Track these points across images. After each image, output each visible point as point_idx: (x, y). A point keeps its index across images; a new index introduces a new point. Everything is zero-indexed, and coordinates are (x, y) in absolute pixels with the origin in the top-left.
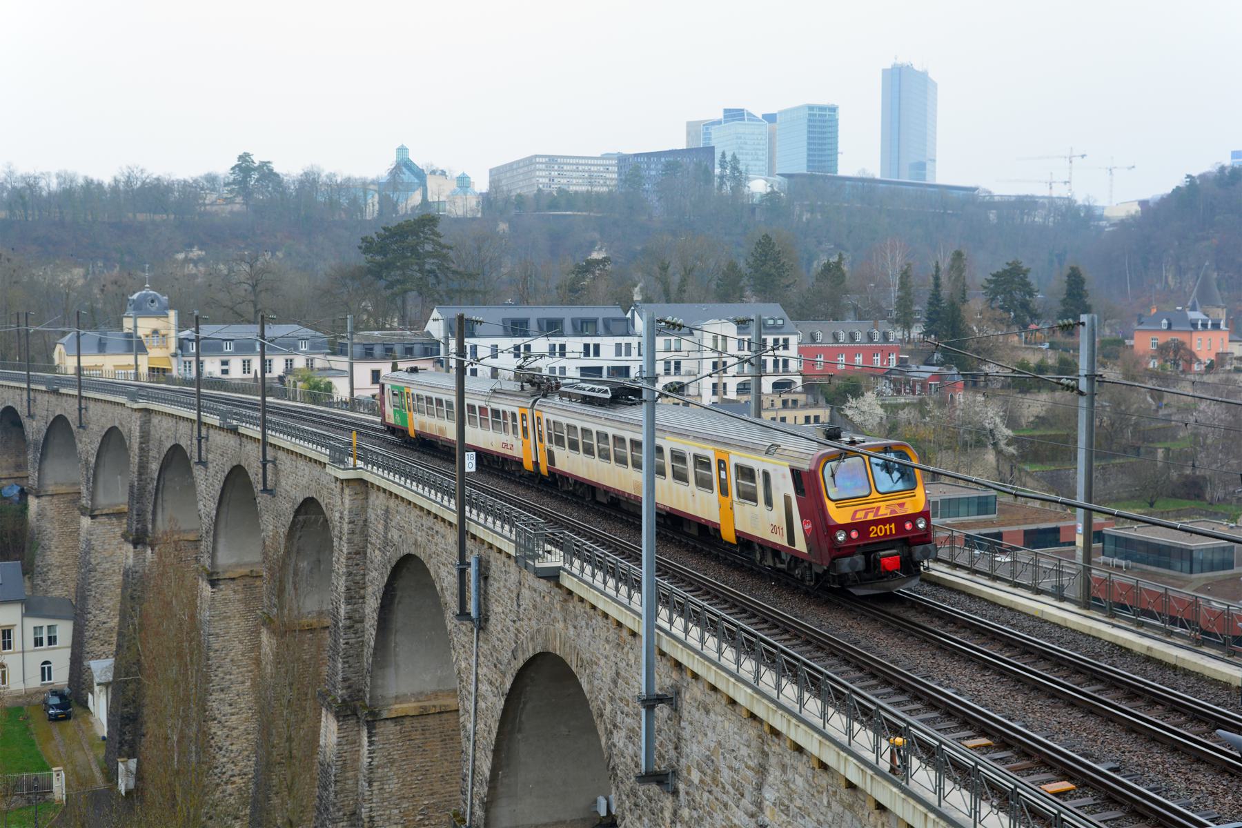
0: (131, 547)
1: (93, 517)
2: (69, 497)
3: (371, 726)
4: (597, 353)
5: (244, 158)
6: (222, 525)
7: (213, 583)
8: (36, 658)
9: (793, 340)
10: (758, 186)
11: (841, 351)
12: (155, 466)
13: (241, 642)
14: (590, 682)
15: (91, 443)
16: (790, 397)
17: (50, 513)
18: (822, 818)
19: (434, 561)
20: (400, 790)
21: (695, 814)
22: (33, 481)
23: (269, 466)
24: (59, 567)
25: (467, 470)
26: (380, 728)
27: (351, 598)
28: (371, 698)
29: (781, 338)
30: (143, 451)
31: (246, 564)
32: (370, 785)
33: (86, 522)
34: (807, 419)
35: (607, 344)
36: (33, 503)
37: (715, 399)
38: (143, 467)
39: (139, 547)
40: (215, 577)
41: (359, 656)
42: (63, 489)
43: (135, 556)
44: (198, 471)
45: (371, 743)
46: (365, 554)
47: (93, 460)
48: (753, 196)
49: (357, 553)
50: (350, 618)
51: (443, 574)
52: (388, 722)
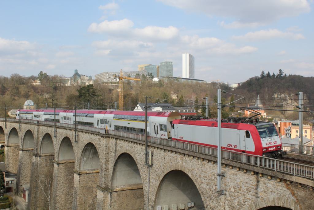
0: (35, 157)
1: (23, 151)
2: (14, 147)
3: (111, 193)
5: (41, 72)
6: (60, 151)
7: (58, 164)
12: (41, 138)
13: (64, 178)
14: (192, 174)
15: (22, 133)
17: (10, 151)
18: (279, 192)
19: (133, 153)
20: (117, 208)
21: (233, 198)
22: (6, 143)
23: (77, 136)
24: (12, 163)
26: (113, 194)
27: (106, 164)
28: (111, 187)
30: (38, 135)
31: (66, 160)
32: (111, 207)
33: (21, 152)
36: (6, 148)
38: (38, 138)
39: (37, 157)
40: (59, 163)
41: (107, 177)
42: (13, 145)
43: (36, 159)
44: (54, 139)
45: (111, 197)
46: (109, 153)
47: (23, 138)
49: (107, 154)
50: (106, 168)
51: (137, 156)
52: (115, 192)
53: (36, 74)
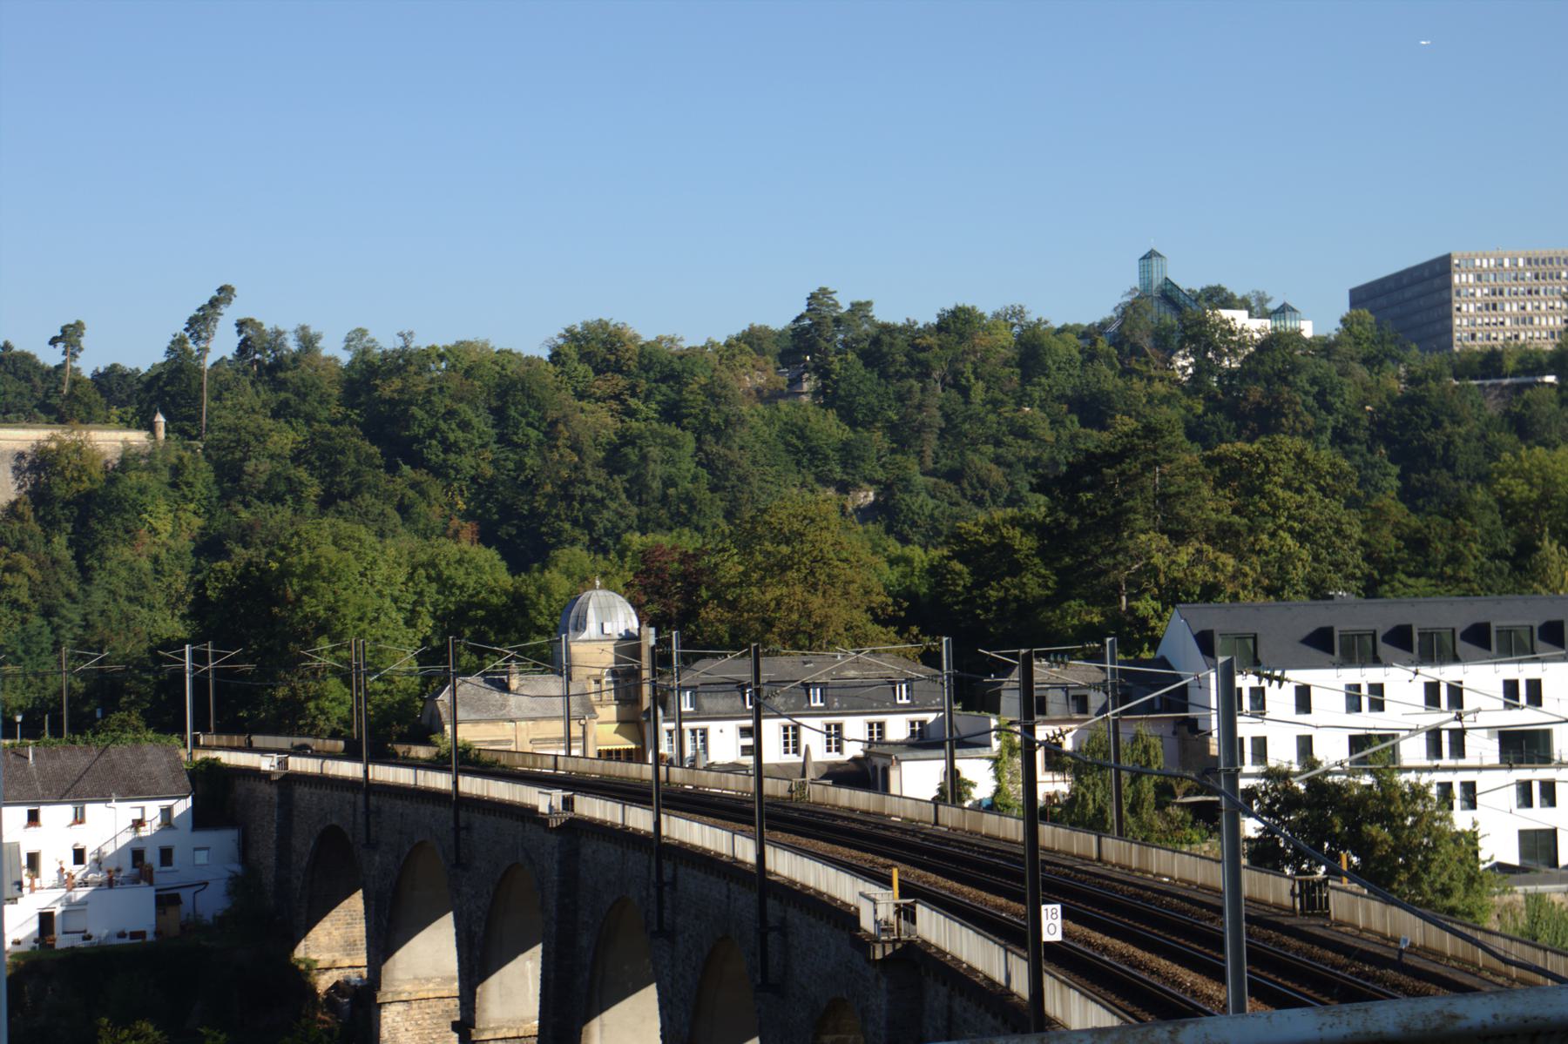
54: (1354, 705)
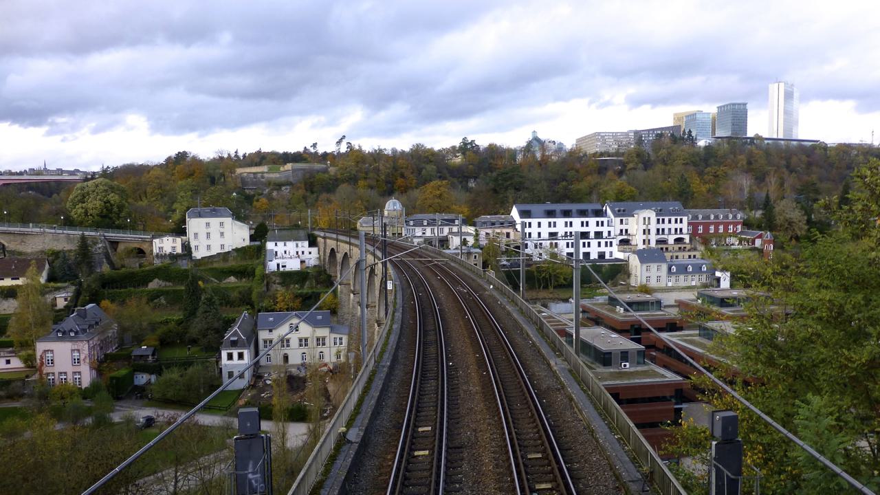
4: (587, 225)
8: (334, 350)
9: (685, 219)
10: (702, 143)
11: (730, 223)
16: (682, 246)
17: (344, 292)
25: (388, 288)
29: (679, 218)
34: (690, 257)
35: (592, 221)
37: (644, 246)
48: (700, 147)
53: (457, 142)
54: (550, 226)
